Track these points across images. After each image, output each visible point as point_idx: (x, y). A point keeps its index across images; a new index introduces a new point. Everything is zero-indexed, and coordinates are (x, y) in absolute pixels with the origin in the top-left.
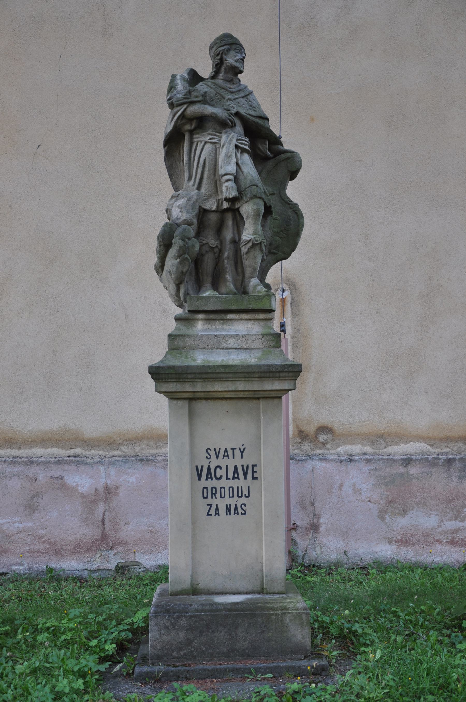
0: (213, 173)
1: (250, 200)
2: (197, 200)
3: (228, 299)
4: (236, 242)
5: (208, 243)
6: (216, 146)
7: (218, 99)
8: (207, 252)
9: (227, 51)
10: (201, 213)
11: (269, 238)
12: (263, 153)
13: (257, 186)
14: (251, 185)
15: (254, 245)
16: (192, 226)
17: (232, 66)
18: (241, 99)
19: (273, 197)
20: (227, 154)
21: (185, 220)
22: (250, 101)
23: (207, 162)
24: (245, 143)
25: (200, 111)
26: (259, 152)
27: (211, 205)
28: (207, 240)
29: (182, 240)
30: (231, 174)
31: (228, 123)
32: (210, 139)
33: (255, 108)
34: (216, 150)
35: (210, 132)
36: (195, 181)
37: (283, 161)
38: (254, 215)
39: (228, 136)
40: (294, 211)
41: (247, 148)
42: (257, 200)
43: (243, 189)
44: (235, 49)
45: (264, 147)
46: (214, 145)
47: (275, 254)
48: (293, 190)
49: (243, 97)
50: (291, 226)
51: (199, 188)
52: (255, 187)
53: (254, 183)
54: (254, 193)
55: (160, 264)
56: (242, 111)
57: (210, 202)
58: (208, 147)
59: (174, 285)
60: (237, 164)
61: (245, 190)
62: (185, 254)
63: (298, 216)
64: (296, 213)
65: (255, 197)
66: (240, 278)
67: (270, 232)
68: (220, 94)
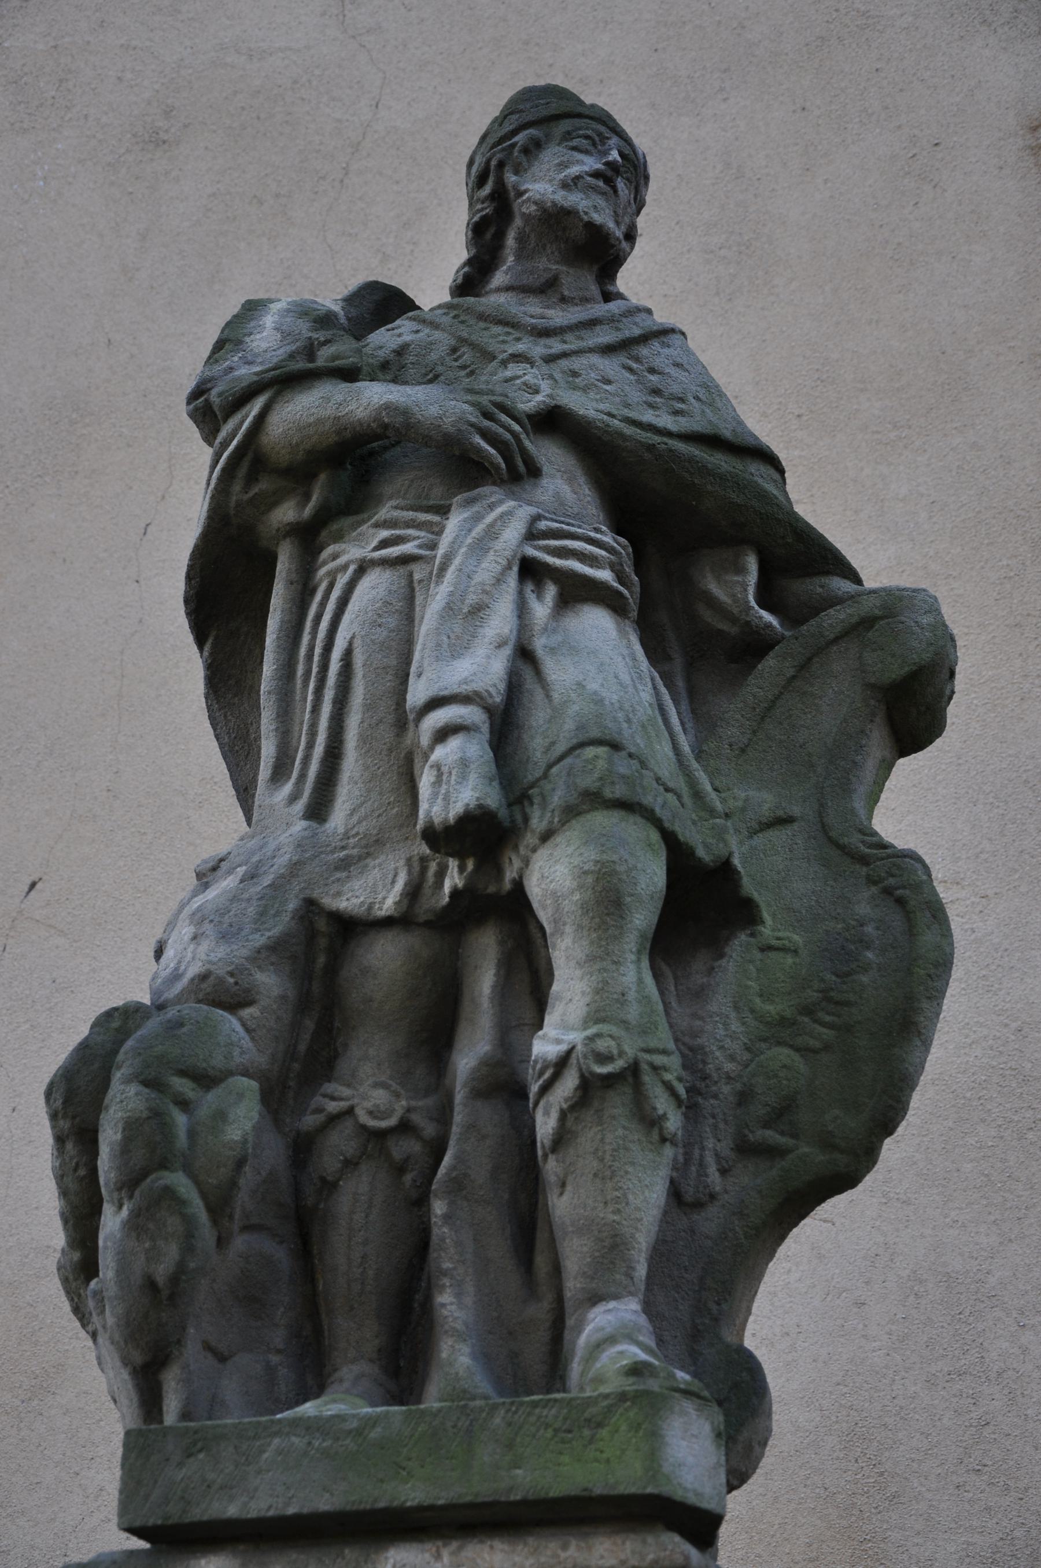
0: (390, 718)
1: (563, 823)
2: (295, 868)
3: (375, 1434)
4: (507, 1087)
5: (350, 1111)
6: (411, 575)
7: (464, 367)
8: (350, 1164)
9: (526, 151)
10: (323, 942)
11: (732, 1058)
12: (733, 620)
13: (615, 746)
14: (582, 745)
15: (590, 1089)
16: (246, 1012)
17: (545, 210)
18: (595, 359)
19: (779, 836)
20: (462, 608)
21: (204, 977)
22: (652, 371)
23: (359, 660)
24: (598, 552)
25: (329, 411)
26: (707, 616)
27: (377, 888)
28: (346, 1092)
29: (146, 1083)
30: (464, 699)
31: (479, 450)
32: (384, 544)
33: (682, 400)
34: (410, 599)
35: (385, 512)
36: (303, 776)
37: (836, 640)
38: (585, 908)
39: (477, 518)
40: (888, 891)
41: (605, 575)
42: (602, 820)
43: (538, 773)
44: (568, 136)
45: (737, 587)
46: (402, 570)
47: (770, 1152)
48: (911, 806)
49: (608, 350)
50: (865, 979)
51: (318, 809)
52: (602, 751)
53: (595, 733)
54: (587, 782)
55: (76, 1256)
56: (584, 405)
57: (374, 874)
58: (373, 588)
59: (125, 1375)
60: (524, 654)
61: (545, 775)
62: (164, 1165)
63: (909, 916)
64: (900, 902)
65: (594, 799)
66: (541, 1310)
67: (735, 1026)
68: (473, 345)
